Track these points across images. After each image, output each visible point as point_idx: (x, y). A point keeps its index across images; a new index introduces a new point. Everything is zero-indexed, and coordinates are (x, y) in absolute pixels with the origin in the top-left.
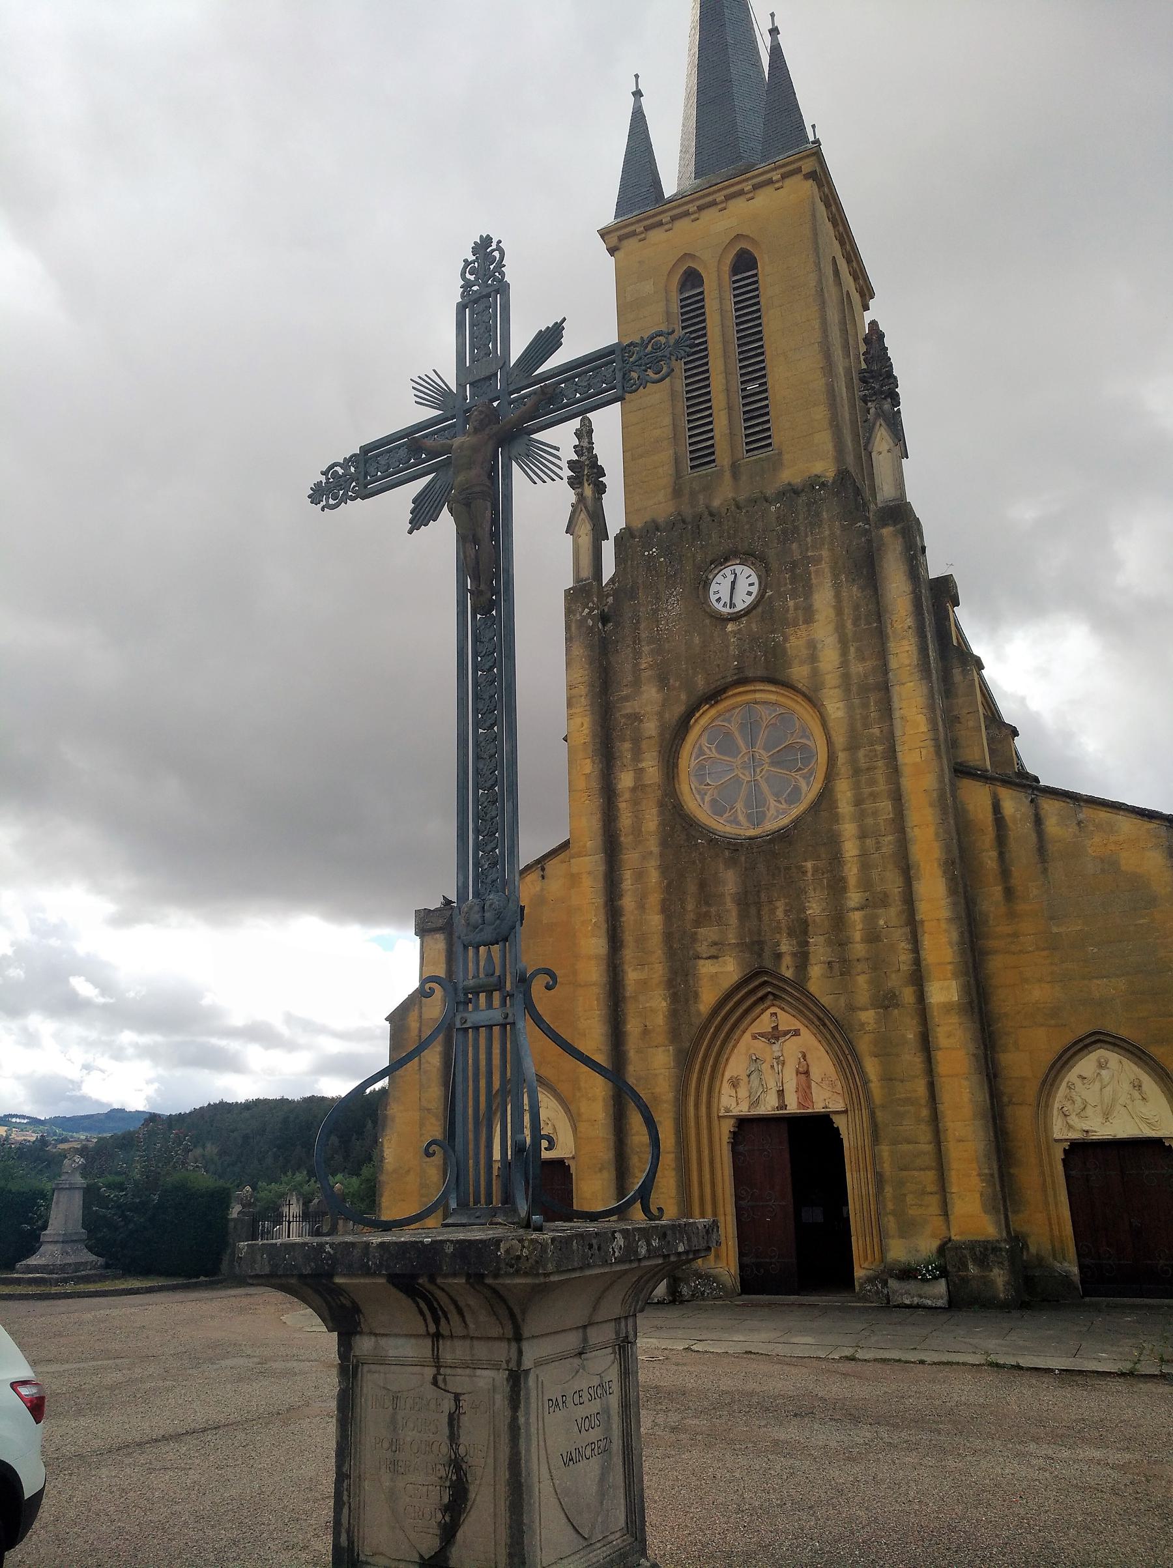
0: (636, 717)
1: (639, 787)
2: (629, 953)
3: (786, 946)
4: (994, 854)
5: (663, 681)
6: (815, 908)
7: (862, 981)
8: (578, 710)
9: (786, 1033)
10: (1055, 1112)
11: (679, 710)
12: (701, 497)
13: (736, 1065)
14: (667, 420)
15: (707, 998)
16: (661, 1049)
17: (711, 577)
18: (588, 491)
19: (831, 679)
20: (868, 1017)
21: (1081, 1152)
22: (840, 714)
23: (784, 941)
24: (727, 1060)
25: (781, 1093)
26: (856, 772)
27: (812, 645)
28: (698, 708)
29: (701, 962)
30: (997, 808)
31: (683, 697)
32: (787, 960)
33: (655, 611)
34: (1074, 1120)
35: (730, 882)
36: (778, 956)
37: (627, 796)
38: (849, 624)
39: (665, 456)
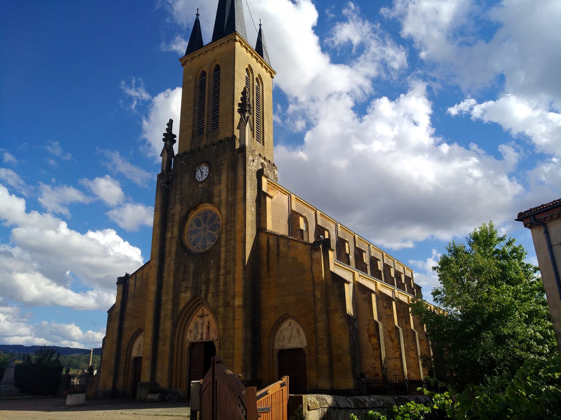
0: (174, 215)
2: (164, 291)
3: (203, 288)
4: (266, 256)
5: (181, 203)
6: (212, 276)
7: (221, 298)
8: (157, 213)
11: (184, 212)
13: (191, 326)
14: (192, 120)
15: (182, 305)
18: (168, 143)
19: (224, 202)
20: (221, 310)
21: (282, 352)
25: (202, 334)
26: (227, 231)
27: (220, 192)
28: (190, 211)
30: (268, 242)
32: (203, 292)
34: (280, 343)
35: (192, 267)
36: (201, 291)
39: (190, 131)
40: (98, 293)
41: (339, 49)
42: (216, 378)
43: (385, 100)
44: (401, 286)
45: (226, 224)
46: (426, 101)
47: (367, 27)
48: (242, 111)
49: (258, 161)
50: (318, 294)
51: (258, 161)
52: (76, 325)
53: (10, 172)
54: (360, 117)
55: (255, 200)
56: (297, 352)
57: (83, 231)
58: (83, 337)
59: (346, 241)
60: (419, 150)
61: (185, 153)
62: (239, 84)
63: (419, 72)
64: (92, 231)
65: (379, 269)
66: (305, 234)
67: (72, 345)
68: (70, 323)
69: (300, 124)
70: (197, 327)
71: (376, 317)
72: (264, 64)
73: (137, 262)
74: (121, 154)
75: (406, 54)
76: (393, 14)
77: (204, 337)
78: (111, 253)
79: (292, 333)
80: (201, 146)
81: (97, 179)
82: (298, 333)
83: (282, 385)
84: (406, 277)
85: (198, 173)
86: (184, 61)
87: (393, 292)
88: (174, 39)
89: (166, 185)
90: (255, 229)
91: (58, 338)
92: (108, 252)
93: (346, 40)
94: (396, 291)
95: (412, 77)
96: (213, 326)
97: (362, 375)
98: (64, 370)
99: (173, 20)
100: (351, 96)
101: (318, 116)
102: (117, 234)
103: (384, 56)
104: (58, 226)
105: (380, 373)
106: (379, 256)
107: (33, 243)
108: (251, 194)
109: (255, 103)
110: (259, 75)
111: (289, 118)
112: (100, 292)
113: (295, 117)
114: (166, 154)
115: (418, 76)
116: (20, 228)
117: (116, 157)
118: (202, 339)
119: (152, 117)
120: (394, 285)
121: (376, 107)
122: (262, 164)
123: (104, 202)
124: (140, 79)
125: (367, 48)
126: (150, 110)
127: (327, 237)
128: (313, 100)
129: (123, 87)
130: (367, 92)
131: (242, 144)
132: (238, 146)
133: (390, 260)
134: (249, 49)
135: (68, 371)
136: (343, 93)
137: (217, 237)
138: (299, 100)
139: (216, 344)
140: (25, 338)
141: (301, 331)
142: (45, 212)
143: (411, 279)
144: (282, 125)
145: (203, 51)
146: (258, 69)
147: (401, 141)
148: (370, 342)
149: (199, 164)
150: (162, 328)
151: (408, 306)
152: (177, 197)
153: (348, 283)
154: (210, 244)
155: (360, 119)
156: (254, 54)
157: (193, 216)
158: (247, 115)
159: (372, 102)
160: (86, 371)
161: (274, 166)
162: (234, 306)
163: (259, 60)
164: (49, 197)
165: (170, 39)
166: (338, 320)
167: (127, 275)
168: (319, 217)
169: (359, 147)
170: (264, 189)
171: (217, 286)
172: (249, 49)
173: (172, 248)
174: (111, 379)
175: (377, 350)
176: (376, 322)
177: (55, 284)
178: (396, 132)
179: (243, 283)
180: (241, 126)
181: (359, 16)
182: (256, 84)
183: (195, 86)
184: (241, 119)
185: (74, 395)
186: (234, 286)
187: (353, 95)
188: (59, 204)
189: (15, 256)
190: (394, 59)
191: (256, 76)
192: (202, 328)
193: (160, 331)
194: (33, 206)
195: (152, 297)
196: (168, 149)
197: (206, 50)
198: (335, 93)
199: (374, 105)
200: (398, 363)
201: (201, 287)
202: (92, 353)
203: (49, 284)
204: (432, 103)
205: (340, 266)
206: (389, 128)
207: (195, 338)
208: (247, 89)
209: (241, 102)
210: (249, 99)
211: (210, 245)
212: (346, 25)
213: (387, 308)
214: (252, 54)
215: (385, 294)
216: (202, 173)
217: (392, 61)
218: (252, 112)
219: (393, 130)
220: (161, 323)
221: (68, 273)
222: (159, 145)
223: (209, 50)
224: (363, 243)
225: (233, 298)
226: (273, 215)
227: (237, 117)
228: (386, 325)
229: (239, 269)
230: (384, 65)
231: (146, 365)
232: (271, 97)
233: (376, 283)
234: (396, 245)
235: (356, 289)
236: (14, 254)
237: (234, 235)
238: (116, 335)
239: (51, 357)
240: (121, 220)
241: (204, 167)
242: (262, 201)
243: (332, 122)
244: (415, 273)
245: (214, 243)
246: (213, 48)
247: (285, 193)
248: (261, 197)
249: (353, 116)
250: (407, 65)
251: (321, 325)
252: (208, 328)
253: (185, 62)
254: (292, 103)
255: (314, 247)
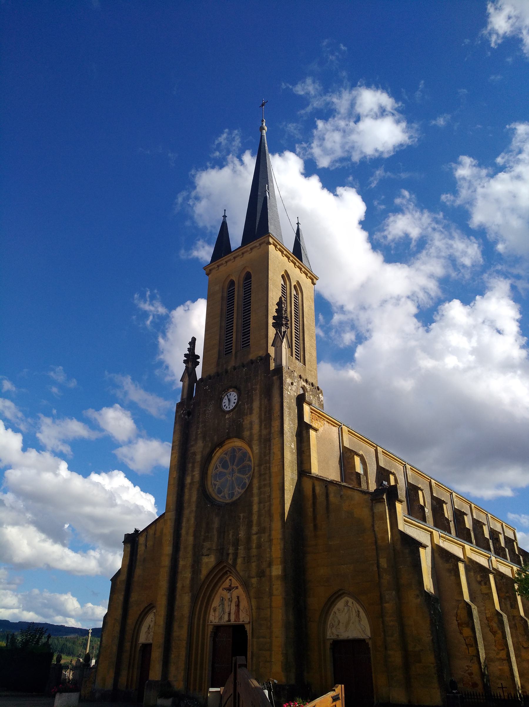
0: (194, 454)
1: (192, 483)
2: (181, 553)
4: (312, 509)
6: (242, 534)
7: (254, 564)
8: (175, 451)
9: (234, 588)
10: (328, 626)
11: (208, 450)
12: (225, 366)
13: (216, 603)
14: (218, 337)
15: (204, 572)
16: (187, 594)
17: (223, 396)
18: (190, 365)
19: (256, 437)
20: (254, 581)
22: (257, 451)
23: (231, 548)
24: (213, 599)
25: (229, 614)
26: (260, 475)
27: (251, 423)
28: (215, 449)
29: (203, 557)
31: (210, 445)
32: (231, 556)
33: (205, 410)
34: (334, 630)
35: (216, 523)
36: (228, 554)
37: (188, 486)
38: (263, 415)
39: (216, 351)
40: (101, 554)
41: (393, 245)
42: (239, 689)
43: (456, 304)
44: (499, 552)
45: (260, 465)
46: (512, 302)
47: (426, 218)
48: (277, 325)
49: (298, 384)
50: (384, 563)
51: (298, 384)
52: (73, 595)
53: (8, 403)
54: (426, 326)
55: (295, 434)
56: (357, 644)
57: (86, 475)
58: (81, 612)
59: (420, 489)
60: (507, 366)
61: (210, 377)
62: (274, 293)
63: (499, 267)
64: (96, 473)
65: (467, 526)
66: (363, 479)
67: (67, 622)
68: (66, 593)
69: (348, 337)
70: (223, 604)
71: (466, 597)
72: (303, 269)
73: (149, 513)
74: (133, 379)
75: (479, 247)
76: (458, 202)
77: (233, 617)
78: (118, 502)
79: (349, 617)
80: (229, 368)
81: (104, 409)
82: (359, 616)
83: (335, 699)
84: (506, 538)
85: (225, 401)
86: (209, 269)
87: (489, 560)
88: (196, 244)
89: (186, 417)
90: (296, 472)
91: (51, 612)
92: (115, 500)
93: (401, 234)
94: (493, 558)
95: (490, 275)
96: (244, 603)
97: (453, 685)
98: (55, 658)
99: (194, 222)
100: (413, 300)
101: (370, 326)
102: (125, 477)
103: (451, 251)
104: (57, 468)
105: (479, 682)
106: (465, 509)
107: (28, 488)
108: (290, 426)
109: (293, 314)
110: (298, 282)
111: (334, 330)
112: (103, 551)
113: (341, 327)
114: (187, 379)
115: (498, 272)
116: (14, 469)
117: (127, 382)
118: (229, 620)
119: (169, 335)
120: (489, 550)
121: (445, 313)
122: (303, 388)
123: (113, 437)
124: (156, 291)
125: (430, 242)
126: (167, 326)
127: (392, 483)
128: (363, 308)
129: (136, 302)
130: (433, 294)
131: (278, 364)
132: (272, 366)
133: (481, 514)
134: (285, 252)
135: (59, 659)
136: (402, 297)
137: (247, 482)
138: (345, 309)
139: (248, 628)
140: (11, 611)
141: (363, 614)
142: (43, 451)
143: (513, 541)
144: (325, 339)
145: (232, 257)
146: (296, 274)
147: (482, 355)
148: (461, 633)
149: (226, 390)
150: (177, 603)
151: (512, 581)
152: (199, 431)
153: (425, 547)
154: (239, 491)
155: (426, 328)
156: (291, 258)
157: (218, 454)
158: (283, 329)
159: (439, 307)
160: (81, 660)
161: (318, 389)
162: (270, 576)
163: (297, 264)
164: (49, 432)
165: (190, 244)
166: (413, 601)
167: (136, 531)
168: (380, 456)
169: (427, 363)
170: (307, 419)
171: (248, 549)
172: (285, 252)
173: (192, 496)
174: (112, 674)
175: (472, 646)
176: (467, 604)
177: (51, 540)
178: (474, 343)
179: (282, 546)
180: (277, 343)
181: (416, 206)
182: (294, 292)
183: (222, 297)
184: (276, 334)
185: (64, 694)
186: (271, 549)
187: (415, 298)
188: (60, 441)
189: (7, 504)
190: (464, 253)
191: (294, 283)
192: (230, 606)
193: (176, 608)
194: (30, 443)
195: (166, 561)
196: (190, 372)
197: (234, 256)
198: (391, 298)
199: (442, 311)
200: (506, 668)
201: (228, 549)
202: (90, 635)
203: (44, 541)
204: (519, 306)
205: (412, 524)
206: (465, 339)
207: (221, 618)
208: (283, 299)
209: (276, 314)
210: (286, 310)
211: (239, 493)
212: (400, 216)
213: (483, 583)
214: (289, 258)
215: (477, 563)
216: (230, 401)
217: (462, 256)
218: (289, 325)
219: (470, 341)
220: (177, 597)
221: (66, 526)
222: (178, 368)
223: (238, 256)
224: (442, 490)
225: (270, 565)
226: (318, 453)
227: (272, 332)
228: (483, 608)
229: (277, 526)
230: (452, 261)
231: (157, 654)
232: (313, 307)
233: (463, 547)
234: (488, 493)
235: (436, 555)
236: (7, 503)
237: (270, 480)
238: (120, 611)
239: (40, 638)
240: (132, 459)
241: (232, 393)
242: (305, 434)
243: (389, 335)
244: (518, 531)
245: (244, 490)
246: (243, 254)
247: (334, 424)
248: (303, 430)
249: (417, 325)
250: (481, 260)
251: (389, 606)
252: (238, 606)
253: (210, 270)
254: (337, 313)
255: (376, 497)
